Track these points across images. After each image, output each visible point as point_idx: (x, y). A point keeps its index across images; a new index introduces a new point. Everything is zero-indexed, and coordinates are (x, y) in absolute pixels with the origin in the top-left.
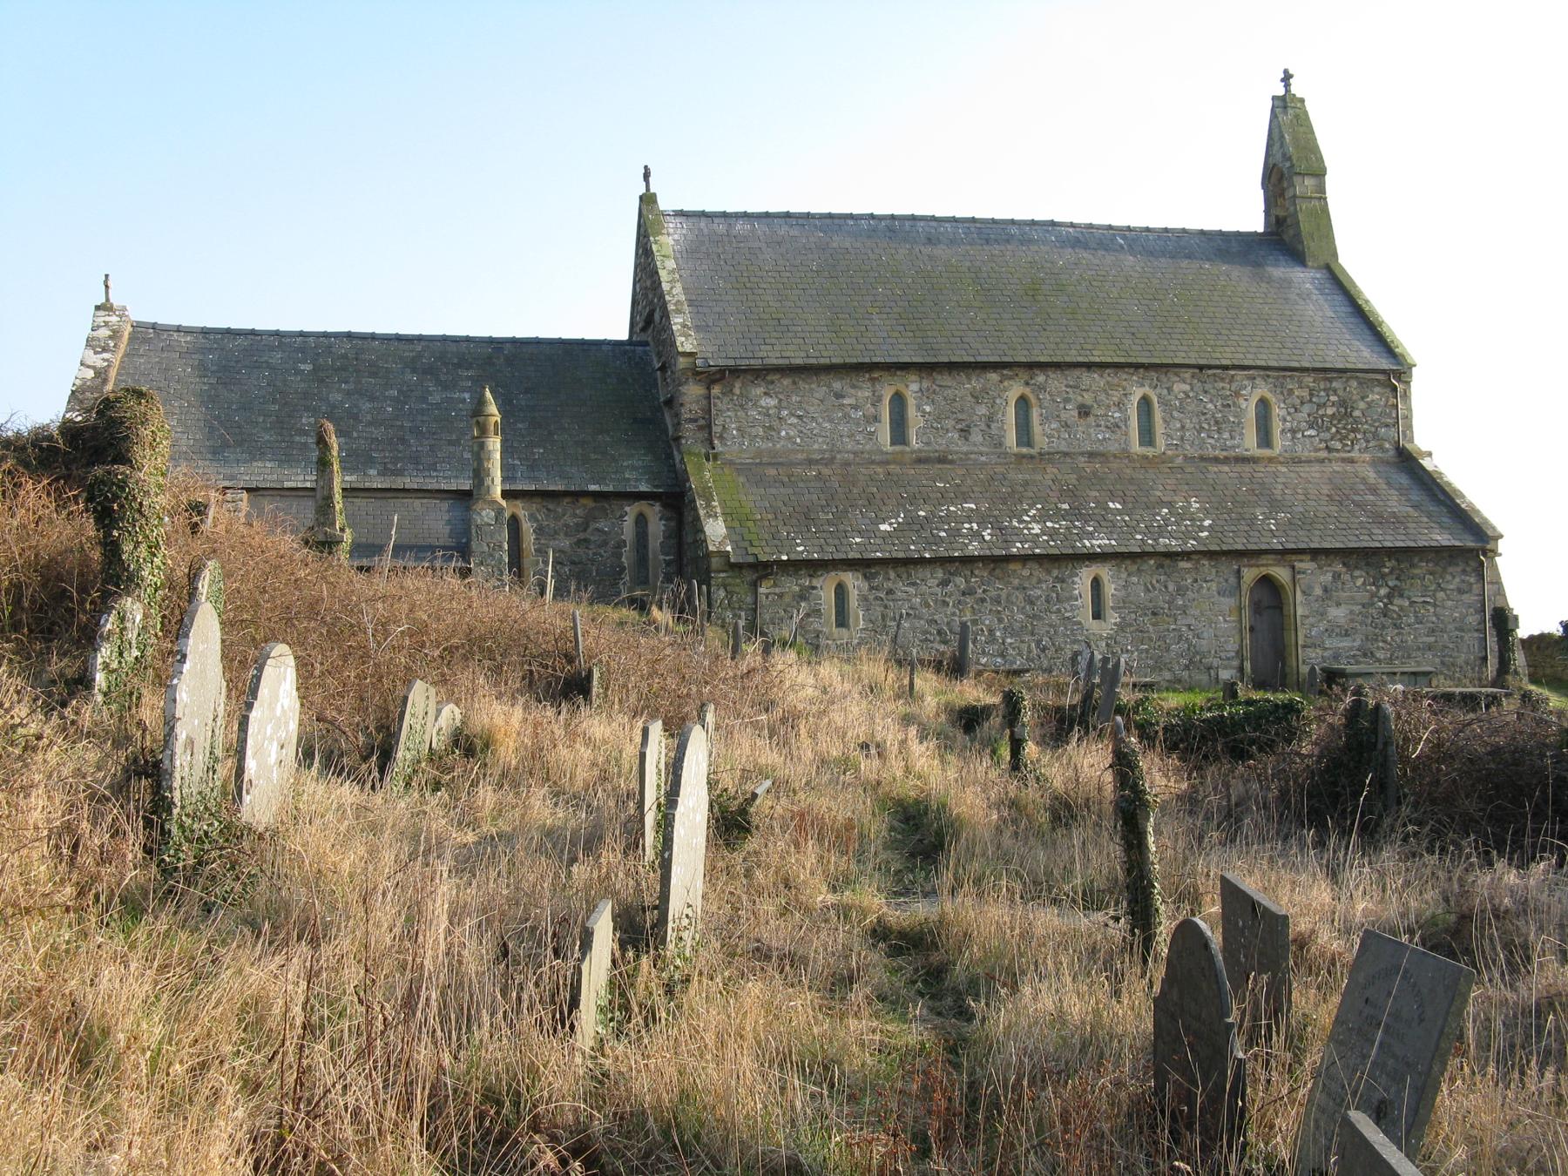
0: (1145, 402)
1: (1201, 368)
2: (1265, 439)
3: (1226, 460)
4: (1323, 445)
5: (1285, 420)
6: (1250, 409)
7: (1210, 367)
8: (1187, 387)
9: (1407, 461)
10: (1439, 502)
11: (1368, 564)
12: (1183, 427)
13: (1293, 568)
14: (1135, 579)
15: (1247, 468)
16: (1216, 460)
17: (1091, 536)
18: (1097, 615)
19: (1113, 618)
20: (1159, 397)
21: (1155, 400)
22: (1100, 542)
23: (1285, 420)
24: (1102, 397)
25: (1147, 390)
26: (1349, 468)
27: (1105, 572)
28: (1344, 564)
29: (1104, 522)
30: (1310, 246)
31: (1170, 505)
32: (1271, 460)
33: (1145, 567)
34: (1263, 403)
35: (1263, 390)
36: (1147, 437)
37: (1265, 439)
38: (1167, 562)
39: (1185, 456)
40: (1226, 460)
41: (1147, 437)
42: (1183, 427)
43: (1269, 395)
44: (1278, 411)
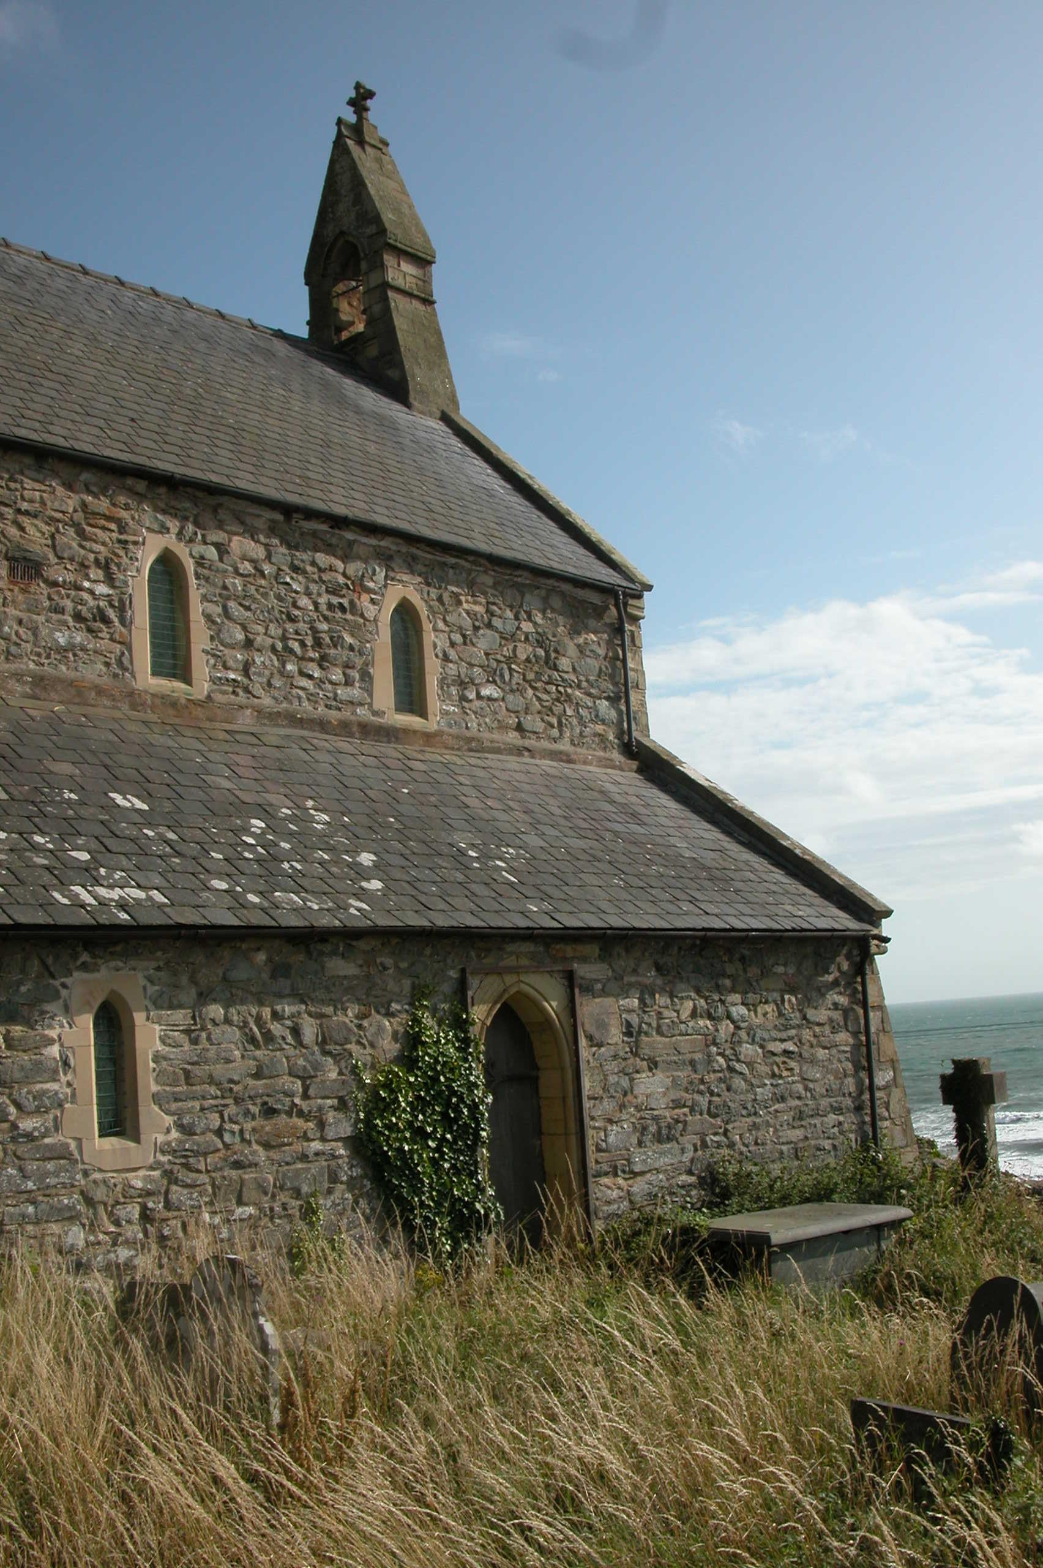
0: (167, 569)
1: (288, 510)
2: (412, 698)
3: (344, 728)
4: (513, 721)
5: (446, 658)
6: (382, 616)
7: (311, 514)
8: (261, 553)
9: (658, 769)
10: (242, 938)
11: (697, 970)
12: (249, 644)
13: (570, 977)
14: (216, 1011)
15: (390, 750)
16: (323, 725)
17: (88, 874)
18: (119, 1120)
19: (158, 1125)
20: (200, 561)
21: (190, 566)
22: (116, 895)
23: (446, 658)
24: (69, 538)
25: (169, 541)
26: (566, 769)
27: (129, 980)
28: (659, 968)
29: (114, 843)
30: (418, 375)
31: (265, 811)
32: (429, 738)
33: (241, 973)
34: (405, 613)
35: (406, 588)
36: (173, 658)
37: (412, 698)
38: (298, 958)
39: (259, 711)
40: (344, 728)
41: (173, 658)
42: (249, 644)
43: (416, 599)
44: (433, 639)
